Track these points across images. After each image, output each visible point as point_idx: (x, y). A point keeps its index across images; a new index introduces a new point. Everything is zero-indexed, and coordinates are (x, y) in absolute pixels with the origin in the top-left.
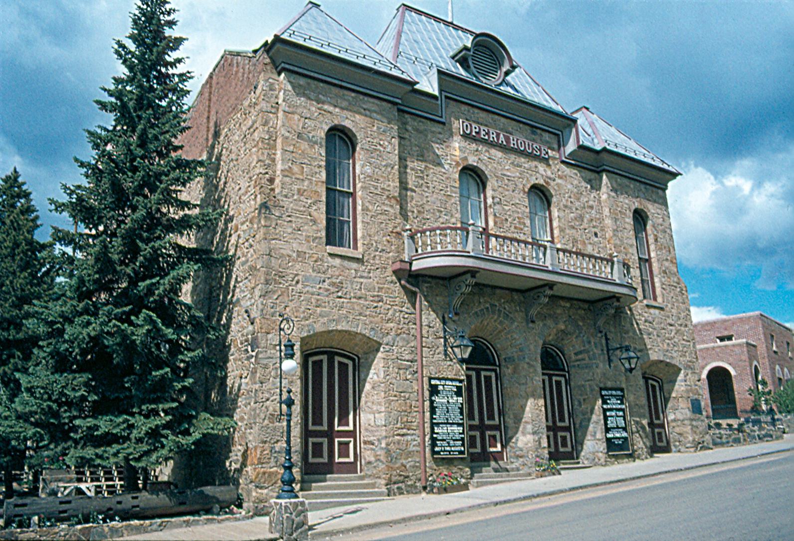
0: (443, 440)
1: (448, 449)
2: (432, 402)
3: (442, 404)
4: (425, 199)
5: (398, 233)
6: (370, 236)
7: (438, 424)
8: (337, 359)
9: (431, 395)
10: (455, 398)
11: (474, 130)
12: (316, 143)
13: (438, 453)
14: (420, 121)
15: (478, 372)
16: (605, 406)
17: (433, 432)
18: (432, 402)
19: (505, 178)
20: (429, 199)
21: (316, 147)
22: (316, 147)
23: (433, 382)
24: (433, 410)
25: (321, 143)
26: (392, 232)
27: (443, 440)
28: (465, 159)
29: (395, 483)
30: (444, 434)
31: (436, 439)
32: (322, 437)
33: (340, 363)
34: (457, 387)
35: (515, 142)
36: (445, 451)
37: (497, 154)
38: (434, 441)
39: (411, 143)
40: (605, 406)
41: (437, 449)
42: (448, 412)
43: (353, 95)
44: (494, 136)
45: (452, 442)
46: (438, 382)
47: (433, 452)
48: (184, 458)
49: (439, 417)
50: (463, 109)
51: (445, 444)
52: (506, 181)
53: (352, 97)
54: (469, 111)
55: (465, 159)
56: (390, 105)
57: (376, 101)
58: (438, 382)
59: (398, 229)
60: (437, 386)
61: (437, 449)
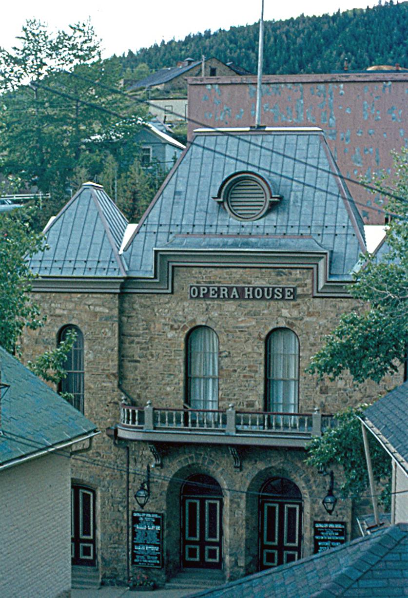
0: (141, 555)
1: (145, 561)
2: (134, 529)
3: (142, 530)
4: (149, 367)
5: (116, 403)
6: (91, 408)
7: (138, 544)
8: (81, 491)
9: (133, 524)
10: (153, 527)
11: (202, 292)
12: (49, 344)
13: (137, 563)
14: (147, 297)
15: (202, 502)
16: (317, 537)
17: (133, 549)
18: (134, 529)
19: (237, 330)
20: (152, 366)
21: (49, 347)
22: (49, 347)
23: (135, 515)
24: (134, 534)
25: (53, 343)
26: (110, 403)
27: (141, 555)
28: (194, 321)
29: (108, 578)
30: (142, 550)
31: (136, 554)
32: (205, 504)
33: (84, 494)
34: (155, 518)
35: (251, 293)
36: (142, 562)
37: (230, 306)
38: (134, 555)
39: (138, 319)
40: (317, 537)
41: (136, 561)
42: (146, 536)
43: (79, 295)
44: (225, 292)
45: (149, 557)
46: (139, 515)
47: (133, 563)
48: (272, 455)
49: (138, 539)
50: (193, 272)
51: (143, 557)
52: (239, 333)
53: (79, 298)
54: (200, 273)
55: (194, 321)
56: (111, 296)
57: (99, 296)
58: (139, 515)
59: (116, 399)
60: (138, 517)
61: (136, 561)
